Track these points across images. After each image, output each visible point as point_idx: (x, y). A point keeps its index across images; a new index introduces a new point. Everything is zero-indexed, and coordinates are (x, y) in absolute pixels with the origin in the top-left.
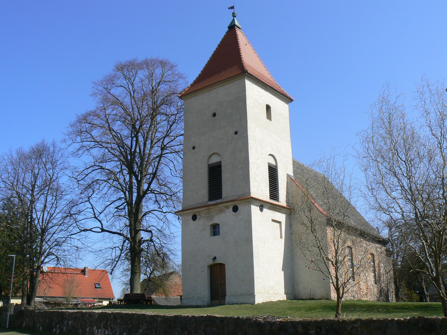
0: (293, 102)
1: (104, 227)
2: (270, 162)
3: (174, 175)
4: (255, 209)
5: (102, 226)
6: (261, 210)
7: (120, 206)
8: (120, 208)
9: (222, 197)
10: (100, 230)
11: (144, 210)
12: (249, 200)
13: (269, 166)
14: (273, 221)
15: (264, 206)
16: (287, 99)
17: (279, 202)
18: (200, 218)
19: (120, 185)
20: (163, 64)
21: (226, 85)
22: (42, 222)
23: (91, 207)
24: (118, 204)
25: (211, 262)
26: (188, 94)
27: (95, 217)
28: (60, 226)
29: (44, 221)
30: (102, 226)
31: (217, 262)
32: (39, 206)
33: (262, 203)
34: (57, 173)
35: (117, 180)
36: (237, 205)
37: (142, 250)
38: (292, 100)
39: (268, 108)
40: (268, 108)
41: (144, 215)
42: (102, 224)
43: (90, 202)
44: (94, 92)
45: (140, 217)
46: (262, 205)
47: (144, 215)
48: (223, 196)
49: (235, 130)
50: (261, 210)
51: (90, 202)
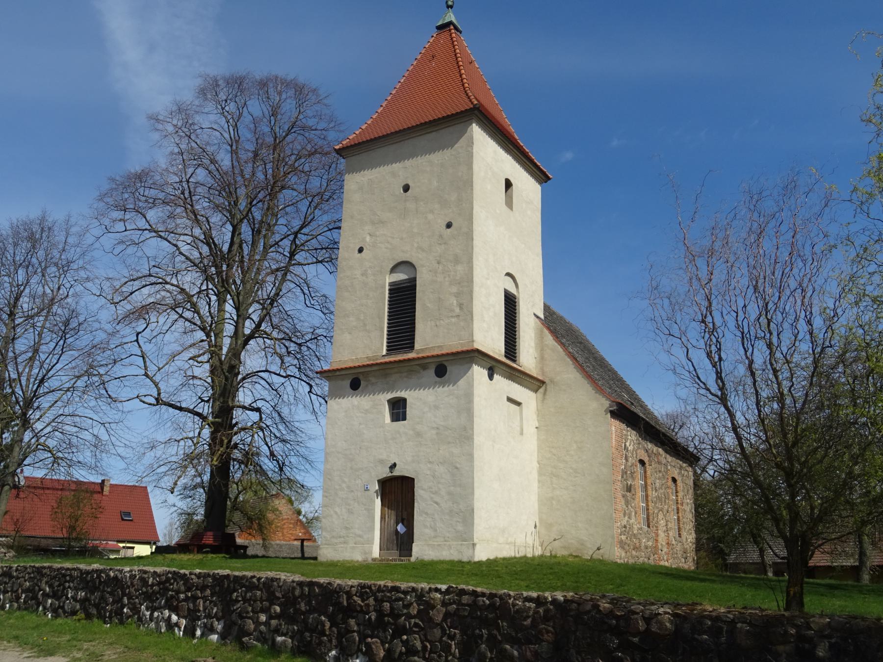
0: (549, 182)
1: (162, 395)
2: (507, 288)
3: (309, 305)
4: (479, 373)
5: (159, 394)
6: (491, 377)
7: (199, 356)
8: (199, 359)
9: (413, 347)
10: (153, 401)
11: (243, 370)
12: (473, 355)
13: (505, 296)
14: (510, 400)
15: (496, 370)
16: (541, 176)
17: (514, 361)
18: (367, 386)
19: (200, 317)
20: (300, 91)
21: (434, 133)
22: (28, 380)
23: (140, 354)
24: (193, 352)
25: (385, 473)
26: (355, 145)
27: (146, 375)
28: (66, 391)
29: (32, 380)
30: (159, 394)
31: (397, 473)
32: (22, 345)
33: (494, 363)
34: (68, 285)
35: (196, 310)
36: (446, 364)
37: (773, 563)
38: (548, 178)
39: (508, 184)
40: (508, 184)
41: (244, 379)
42: (159, 390)
43: (138, 343)
44: (166, 357)
45: (235, 383)
46: (493, 367)
47: (244, 379)
48: (417, 346)
49: (448, 220)
50: (491, 377)
51: (138, 343)
